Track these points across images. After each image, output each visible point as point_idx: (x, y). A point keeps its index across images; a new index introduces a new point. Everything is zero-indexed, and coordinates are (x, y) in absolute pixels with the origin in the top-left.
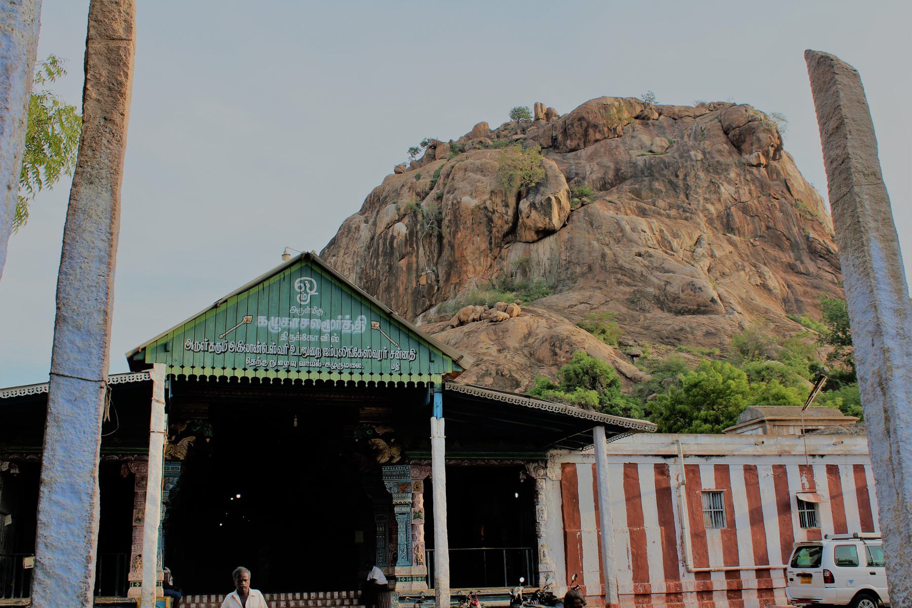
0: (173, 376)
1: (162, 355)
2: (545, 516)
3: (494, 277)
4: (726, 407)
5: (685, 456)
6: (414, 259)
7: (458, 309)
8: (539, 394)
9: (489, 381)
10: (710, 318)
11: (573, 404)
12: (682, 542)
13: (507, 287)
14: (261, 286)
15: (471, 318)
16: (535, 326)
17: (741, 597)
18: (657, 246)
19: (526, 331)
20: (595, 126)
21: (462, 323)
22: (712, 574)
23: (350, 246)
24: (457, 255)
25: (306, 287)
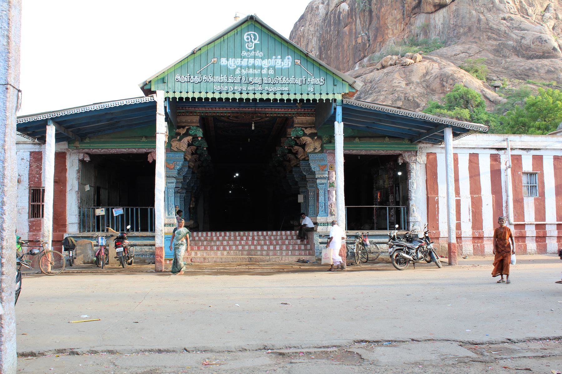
0: (169, 98)
1: (161, 85)
2: (415, 186)
3: (405, 37)
4: (554, 120)
5: (512, 149)
6: (354, 27)
7: (382, 58)
8: (431, 112)
9: (399, 104)
10: (551, 61)
11: (452, 118)
12: (507, 205)
13: (414, 43)
14: (222, 39)
15: (389, 63)
16: (431, 68)
17: (545, 241)
18: (517, 13)
19: (425, 71)
21: (383, 67)
22: (526, 226)
23: (313, 20)
24: (382, 22)
25: (251, 38)
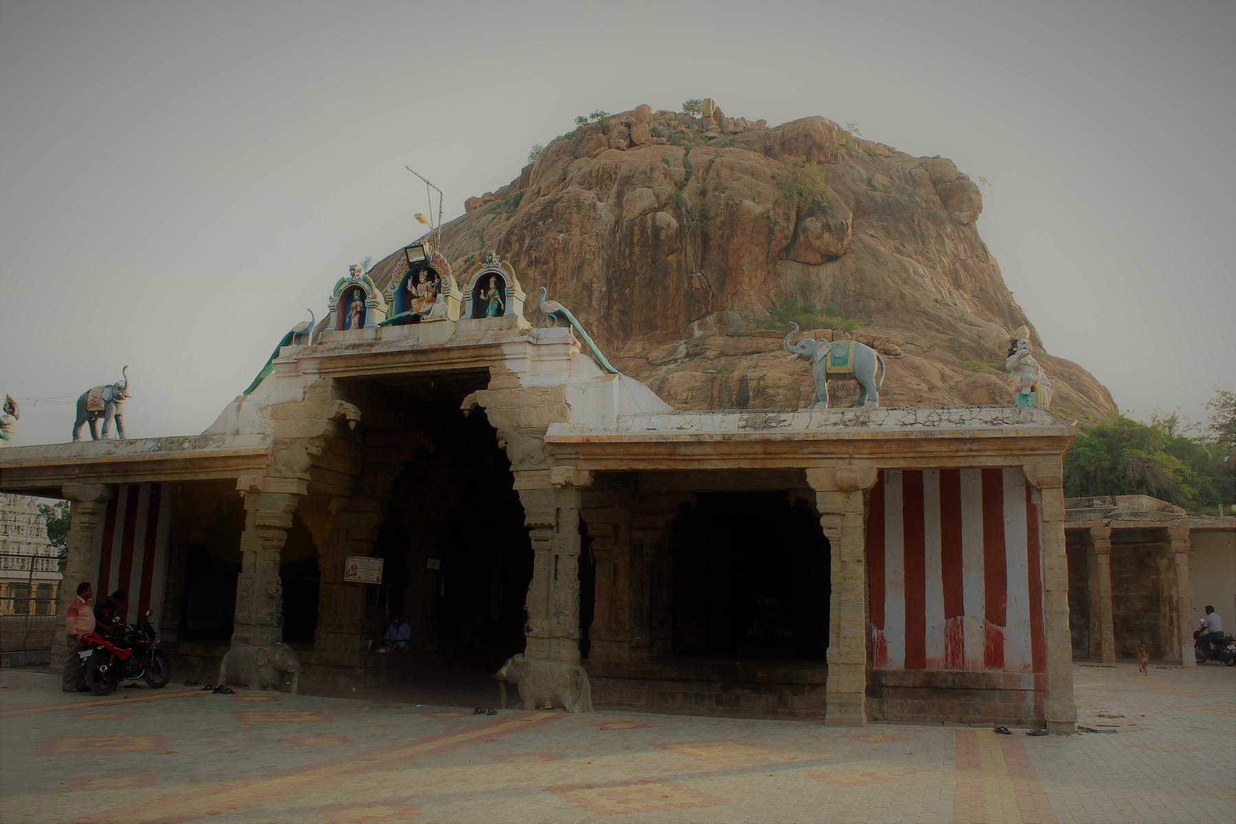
20: (821, 147)
